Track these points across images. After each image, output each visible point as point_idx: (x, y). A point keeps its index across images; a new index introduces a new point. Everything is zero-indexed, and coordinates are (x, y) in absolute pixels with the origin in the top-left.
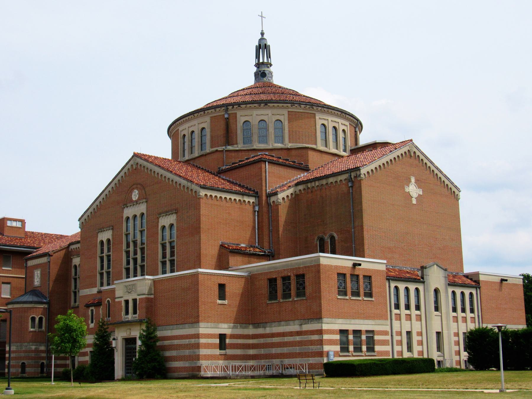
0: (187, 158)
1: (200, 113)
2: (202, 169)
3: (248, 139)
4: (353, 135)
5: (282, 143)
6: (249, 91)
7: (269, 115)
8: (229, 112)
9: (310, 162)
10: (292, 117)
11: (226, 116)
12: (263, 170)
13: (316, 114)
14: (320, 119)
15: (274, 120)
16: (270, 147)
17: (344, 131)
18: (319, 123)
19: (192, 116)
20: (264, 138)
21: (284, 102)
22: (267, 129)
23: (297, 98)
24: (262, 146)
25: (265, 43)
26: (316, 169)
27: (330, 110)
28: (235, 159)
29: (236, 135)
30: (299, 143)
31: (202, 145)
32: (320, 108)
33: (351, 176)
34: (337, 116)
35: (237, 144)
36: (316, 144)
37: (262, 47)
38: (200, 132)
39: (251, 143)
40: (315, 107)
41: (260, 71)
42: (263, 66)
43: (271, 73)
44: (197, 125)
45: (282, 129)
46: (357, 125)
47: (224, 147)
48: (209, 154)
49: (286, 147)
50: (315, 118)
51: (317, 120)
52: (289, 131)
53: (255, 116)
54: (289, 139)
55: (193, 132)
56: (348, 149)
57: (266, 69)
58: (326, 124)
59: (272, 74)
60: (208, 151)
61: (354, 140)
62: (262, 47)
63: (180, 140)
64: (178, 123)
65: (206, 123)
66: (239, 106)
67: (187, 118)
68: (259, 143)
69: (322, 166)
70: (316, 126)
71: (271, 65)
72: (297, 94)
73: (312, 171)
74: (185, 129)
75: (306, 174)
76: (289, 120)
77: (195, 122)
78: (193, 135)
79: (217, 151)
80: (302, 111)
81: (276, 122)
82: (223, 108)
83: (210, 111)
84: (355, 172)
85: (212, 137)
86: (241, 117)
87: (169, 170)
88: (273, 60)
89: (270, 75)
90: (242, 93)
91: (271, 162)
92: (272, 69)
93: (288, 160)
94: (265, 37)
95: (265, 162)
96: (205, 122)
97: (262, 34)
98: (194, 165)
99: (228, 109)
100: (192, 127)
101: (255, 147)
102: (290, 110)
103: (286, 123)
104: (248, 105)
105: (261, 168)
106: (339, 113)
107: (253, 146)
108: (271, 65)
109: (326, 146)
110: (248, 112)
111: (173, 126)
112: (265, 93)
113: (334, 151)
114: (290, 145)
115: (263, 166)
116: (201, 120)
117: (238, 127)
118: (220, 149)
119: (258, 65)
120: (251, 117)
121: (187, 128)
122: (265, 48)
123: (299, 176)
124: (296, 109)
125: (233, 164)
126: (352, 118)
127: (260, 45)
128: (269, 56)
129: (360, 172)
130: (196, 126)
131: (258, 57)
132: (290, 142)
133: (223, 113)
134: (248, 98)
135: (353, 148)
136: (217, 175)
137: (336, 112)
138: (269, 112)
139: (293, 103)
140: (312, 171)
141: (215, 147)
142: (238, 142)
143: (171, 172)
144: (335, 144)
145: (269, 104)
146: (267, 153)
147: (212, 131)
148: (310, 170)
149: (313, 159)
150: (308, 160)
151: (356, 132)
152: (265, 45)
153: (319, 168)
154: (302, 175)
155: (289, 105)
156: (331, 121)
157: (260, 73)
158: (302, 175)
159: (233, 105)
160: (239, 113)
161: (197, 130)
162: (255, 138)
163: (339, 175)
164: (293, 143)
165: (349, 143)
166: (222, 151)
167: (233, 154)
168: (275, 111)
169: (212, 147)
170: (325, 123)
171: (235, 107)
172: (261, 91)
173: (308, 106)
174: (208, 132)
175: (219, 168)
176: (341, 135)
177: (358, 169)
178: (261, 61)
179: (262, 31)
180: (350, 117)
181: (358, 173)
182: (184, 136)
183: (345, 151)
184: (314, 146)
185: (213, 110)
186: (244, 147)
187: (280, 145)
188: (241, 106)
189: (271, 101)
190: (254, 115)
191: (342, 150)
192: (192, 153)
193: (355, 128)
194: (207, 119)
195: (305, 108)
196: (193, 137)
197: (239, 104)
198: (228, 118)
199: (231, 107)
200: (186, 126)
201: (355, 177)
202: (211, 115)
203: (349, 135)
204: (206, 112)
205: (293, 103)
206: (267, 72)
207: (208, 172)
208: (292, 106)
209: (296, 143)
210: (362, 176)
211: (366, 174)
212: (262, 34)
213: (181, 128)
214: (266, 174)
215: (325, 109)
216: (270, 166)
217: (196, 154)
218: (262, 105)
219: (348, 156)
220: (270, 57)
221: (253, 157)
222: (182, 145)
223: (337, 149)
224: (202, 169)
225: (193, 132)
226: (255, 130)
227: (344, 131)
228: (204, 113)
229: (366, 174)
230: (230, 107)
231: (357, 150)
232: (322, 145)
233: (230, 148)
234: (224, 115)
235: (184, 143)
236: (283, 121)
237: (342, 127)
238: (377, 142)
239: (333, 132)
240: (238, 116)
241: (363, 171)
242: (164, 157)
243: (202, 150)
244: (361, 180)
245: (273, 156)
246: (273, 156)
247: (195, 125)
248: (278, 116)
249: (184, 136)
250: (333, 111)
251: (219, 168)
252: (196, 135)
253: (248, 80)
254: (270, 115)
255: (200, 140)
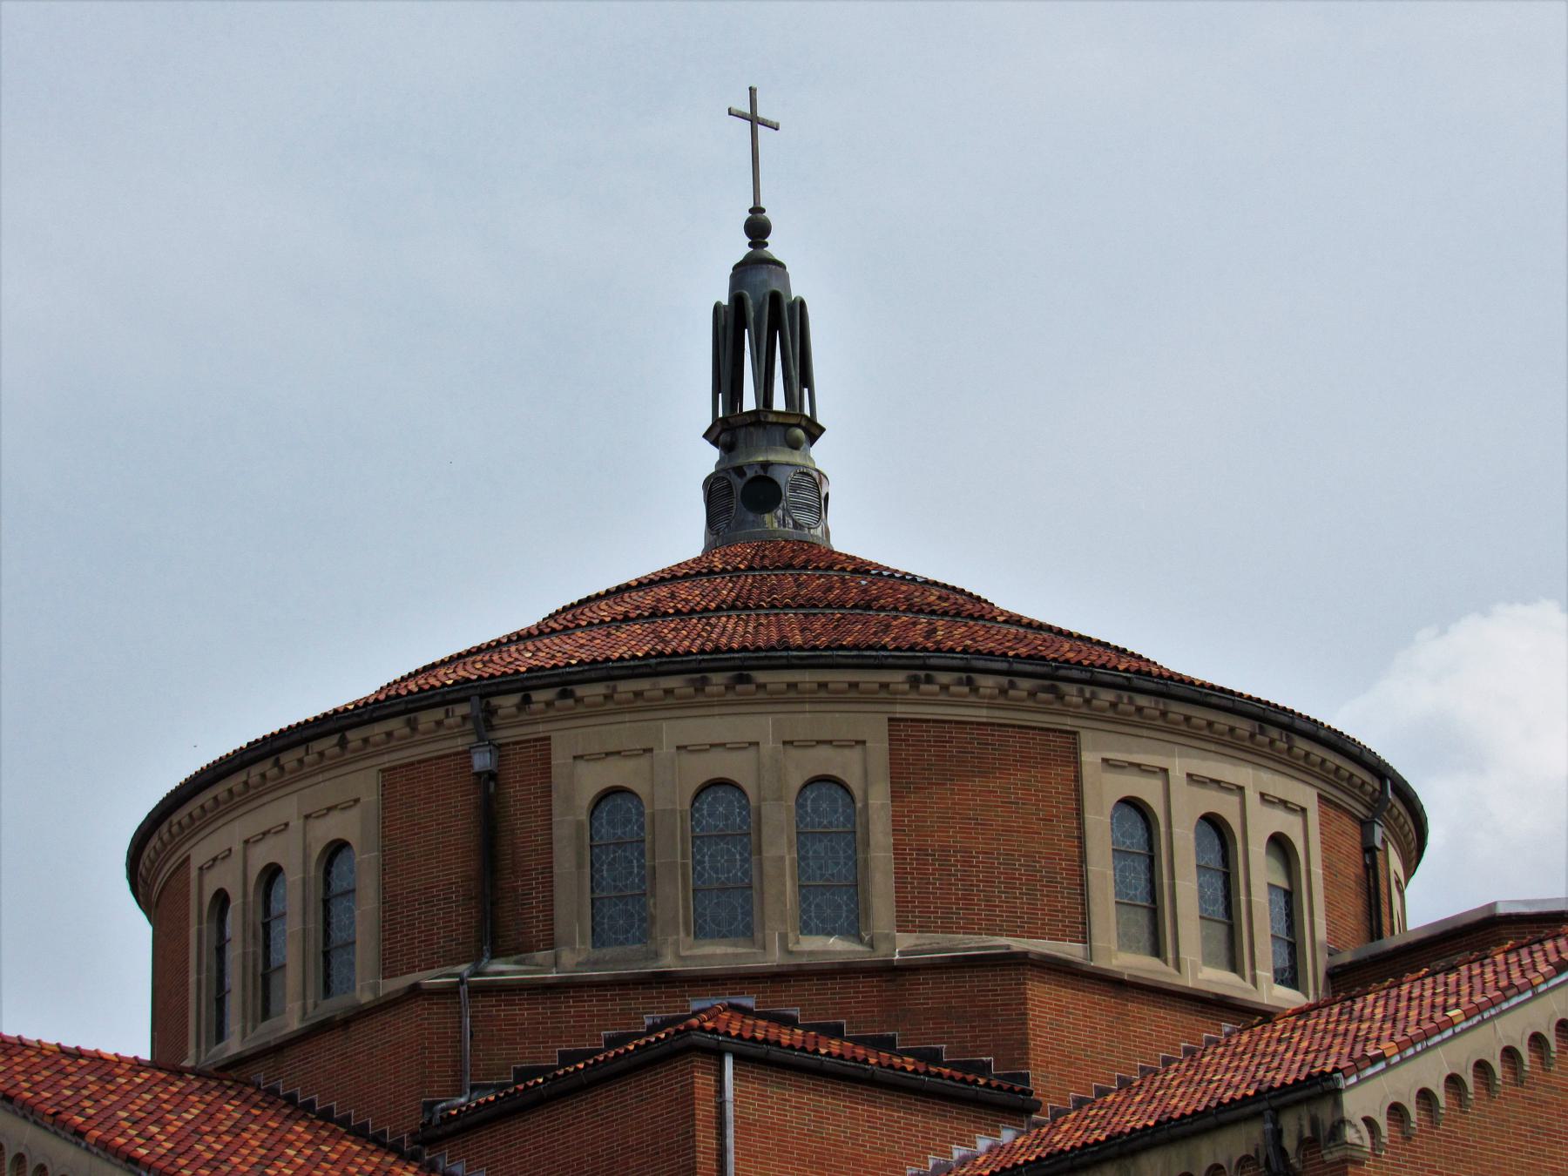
0: (234, 1045)
1: (317, 746)
2: (326, 1115)
3: (622, 909)
4: (1352, 869)
5: (854, 927)
6: (647, 599)
7: (762, 746)
8: (503, 735)
9: (1034, 1056)
10: (917, 759)
11: (482, 761)
12: (704, 1110)
13: (1086, 738)
14: (1112, 769)
15: (796, 781)
16: (774, 958)
17: (1280, 844)
18: (1104, 792)
19: (266, 766)
20: (728, 904)
21: (867, 658)
22: (748, 837)
23: (956, 635)
24: (717, 954)
25: (775, 286)
26: (1080, 1103)
27: (1178, 710)
28: (539, 1043)
29: (548, 884)
30: (967, 930)
31: (329, 956)
32: (1107, 696)
33: (1278, 1134)
34: (1231, 745)
35: (550, 944)
36: (1084, 936)
37: (760, 322)
38: (314, 872)
39: (645, 936)
40: (1070, 690)
41: (740, 471)
42: (758, 434)
43: (813, 482)
44: (296, 823)
45: (854, 838)
46: (1378, 807)
47: (463, 968)
48: (362, 1014)
49: (880, 955)
50: (1077, 764)
51: (1086, 771)
52: (898, 850)
53: (670, 755)
54: (901, 903)
55: (272, 873)
56: (1316, 965)
57: (780, 456)
58: (1155, 802)
59: (817, 486)
60: (365, 997)
61: (1353, 906)
62: (760, 322)
63: (196, 929)
64: (181, 815)
65: (355, 813)
66: (564, 695)
67: (235, 782)
68: (701, 932)
69: (1125, 1083)
70: (1079, 812)
71: (814, 431)
72: (965, 607)
73: (1057, 1113)
74: (223, 856)
75: (1007, 1136)
76: (895, 778)
77: (286, 808)
78: (278, 891)
79: (415, 990)
80: (982, 715)
81: (811, 794)
82: (462, 709)
83: (377, 731)
84: (1304, 1112)
85: (390, 903)
86: (582, 768)
87: (64, 1124)
88: (827, 403)
89: (807, 496)
90: (604, 611)
91: (756, 1059)
92: (820, 454)
93: (886, 1044)
94: (775, 247)
95: (718, 1055)
96: (348, 805)
97: (757, 229)
98: (273, 1091)
99: (491, 712)
100: (271, 841)
101: (668, 962)
102: (901, 710)
103: (879, 799)
104: (626, 687)
105: (687, 1100)
106: (1244, 726)
107: (657, 955)
108: (814, 431)
109: (1157, 950)
110: (622, 732)
111: (154, 842)
112: (766, 594)
113: (1133, 962)
114: (903, 945)
115: (702, 1081)
116: (327, 789)
117: (556, 832)
118: (431, 979)
119: (727, 431)
120: (643, 762)
121: (237, 847)
122: (776, 323)
123: (958, 1152)
124: (940, 705)
125: (522, 1075)
126: (1334, 759)
127: (737, 300)
128: (802, 376)
129: (1338, 1105)
130: (294, 837)
131: (726, 380)
132: (903, 926)
133: (460, 744)
134: (630, 643)
135: (1346, 957)
136: (413, 1157)
137: (1223, 721)
138: (762, 726)
139: (920, 664)
140: (1057, 1113)
141: (412, 969)
142: (559, 931)
143: (79, 1134)
144: (1220, 931)
145: (761, 677)
146: (749, 1002)
147: (388, 866)
148: (1036, 1107)
149: (1064, 1044)
150: (1023, 1044)
151: (1369, 849)
152: (775, 298)
153: (1102, 1092)
154: (983, 1143)
155: (898, 678)
156: (1185, 782)
157: (739, 484)
158: (983, 1143)
159: (524, 684)
160: (566, 740)
161: (293, 855)
162: (672, 897)
163: (1206, 1131)
164: (923, 928)
165: (1318, 926)
166: (450, 992)
167: (522, 1013)
168: (804, 722)
169: (388, 971)
170: (1149, 790)
171: (540, 696)
172: (727, 591)
173: (1025, 684)
174: (364, 873)
175: (429, 1106)
176: (1261, 872)
177: (1320, 1088)
178: (749, 403)
179: (757, 210)
180: (1319, 752)
181: (1325, 1114)
182: (222, 899)
183: (1290, 976)
184: (1071, 950)
185: (396, 725)
186: (595, 964)
187: (836, 947)
188: (580, 691)
189: (778, 657)
190: (665, 750)
191: (1265, 974)
192: (266, 1014)
193: (1366, 826)
194: (363, 783)
195: (1013, 693)
196: (276, 907)
197: (564, 680)
198: (492, 776)
199: (514, 699)
200: (231, 834)
201: (1309, 1144)
202: (388, 760)
203: (1317, 870)
204: (354, 736)
205: (920, 664)
206: (783, 477)
207: (360, 1133)
208: (914, 683)
209: (946, 929)
210: (1350, 1135)
211: (1382, 1122)
212: (757, 229)
213: (200, 854)
214: (721, 1135)
215: (1142, 701)
216: (753, 1087)
217: (291, 1020)
218: (718, 679)
219: (1302, 1013)
220: (806, 380)
221: (653, 1029)
222: (209, 959)
223: (1234, 965)
224: (326, 1115)
225: (272, 873)
226: (671, 851)
227: (1280, 844)
228: (343, 744)
229: (1382, 1122)
230: (508, 703)
231: (1384, 963)
232: (1126, 943)
233: (503, 969)
234: (467, 754)
235: (221, 950)
236: (858, 793)
237: (1263, 823)
238: (1502, 910)
239: (1200, 849)
240: (559, 758)
241: (1362, 1101)
242: (70, 1043)
243: (327, 991)
244: (1344, 1161)
245: (789, 1022)
246: (789, 1022)
247: (286, 831)
248: (824, 752)
249: (222, 899)
250: (1200, 715)
251: (429, 1106)
252: (292, 895)
253: (669, 529)
254: (769, 746)
255: (315, 925)
